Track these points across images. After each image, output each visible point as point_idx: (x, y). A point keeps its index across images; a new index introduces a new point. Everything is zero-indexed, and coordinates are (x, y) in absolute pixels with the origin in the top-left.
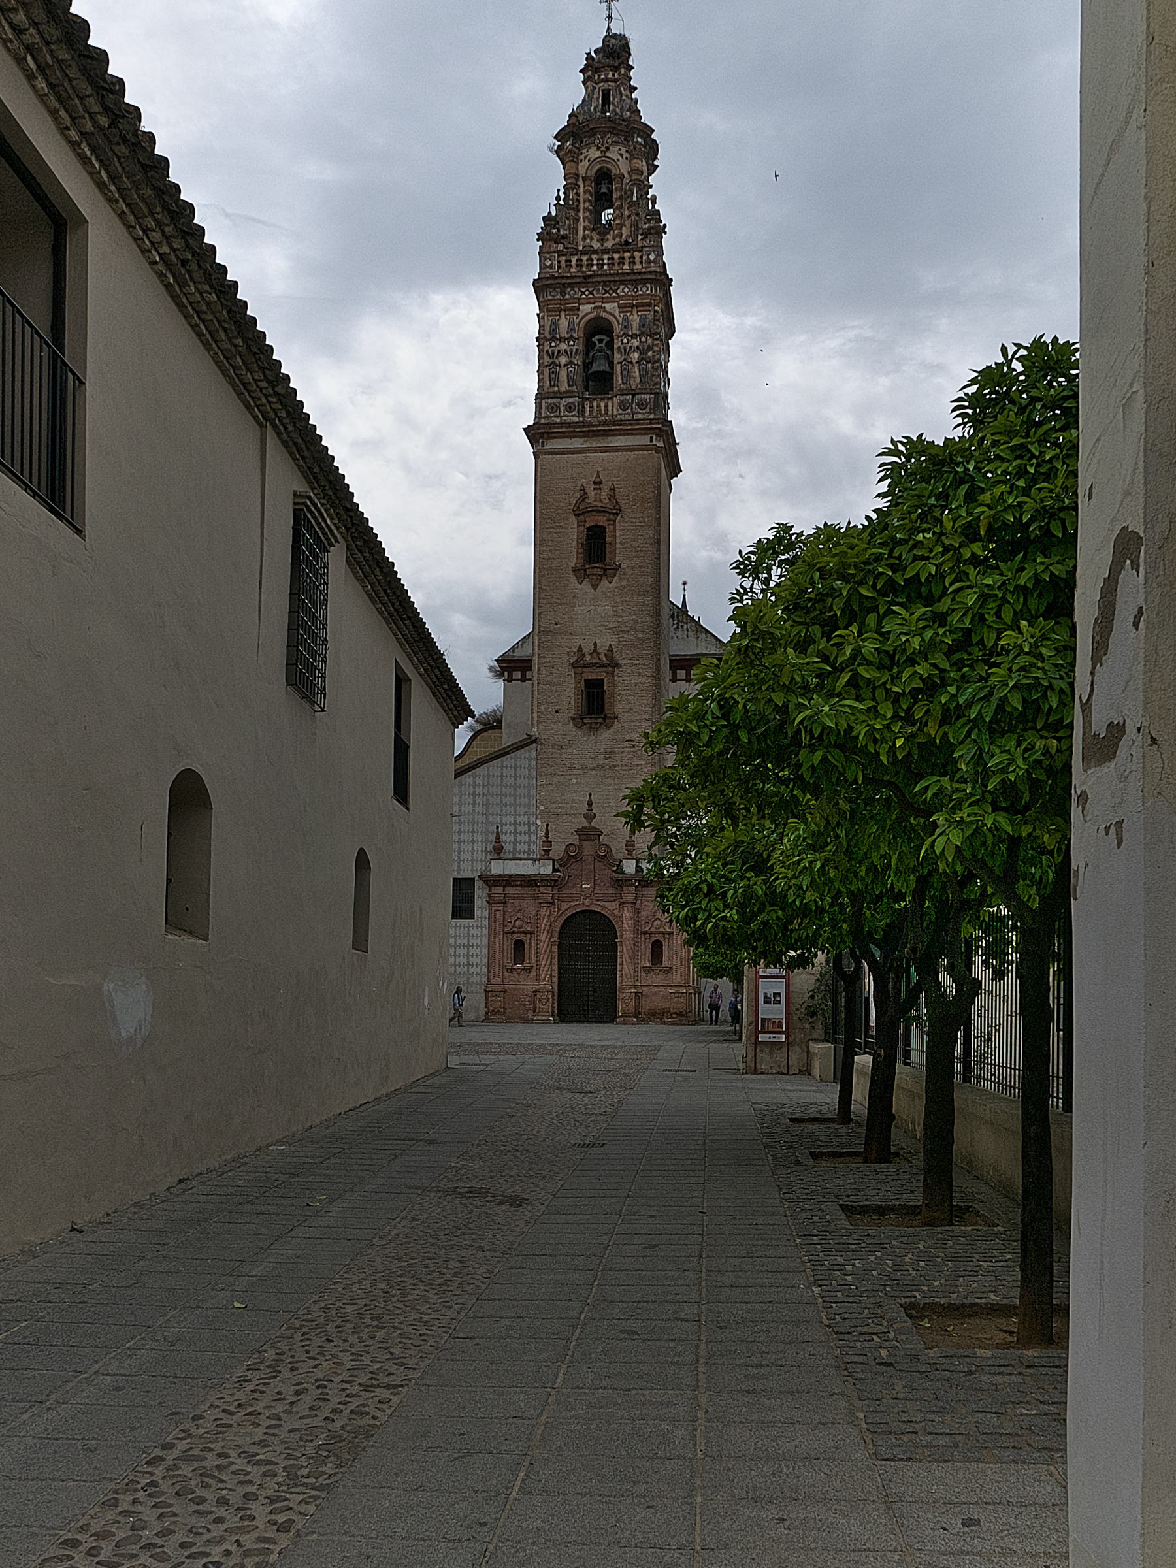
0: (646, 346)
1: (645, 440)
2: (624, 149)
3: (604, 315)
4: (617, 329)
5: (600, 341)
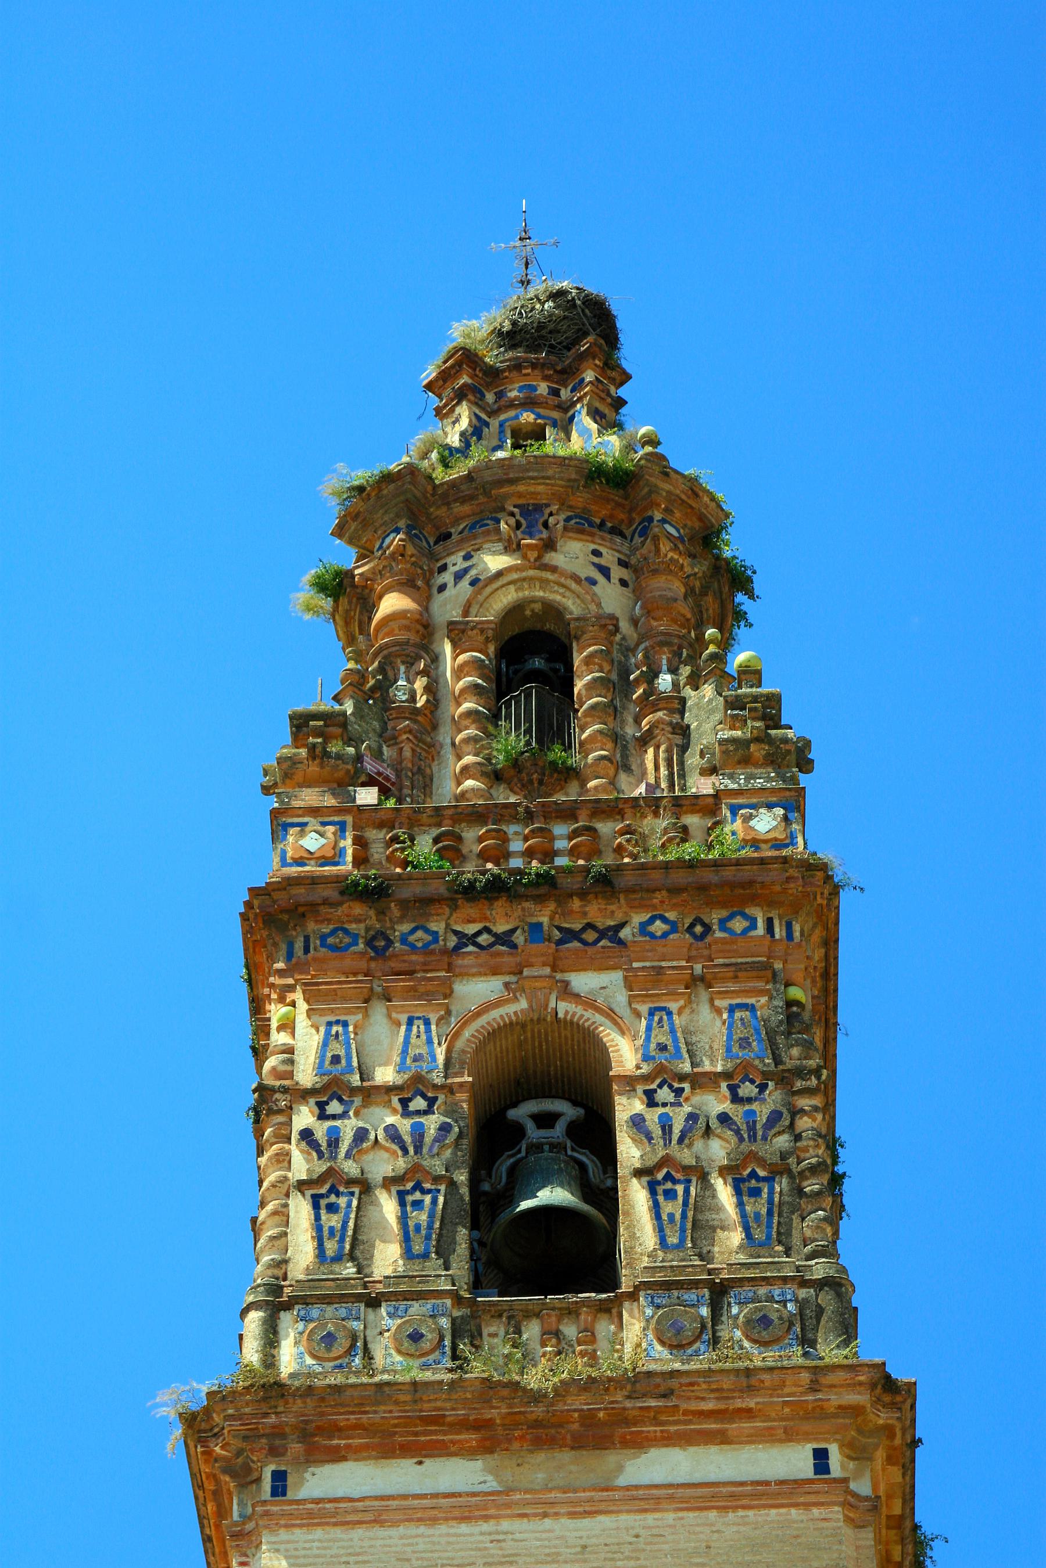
0: (762, 1111)
1: (794, 1461)
2: (609, 558)
3: (564, 1008)
4: (625, 1054)
5: (546, 1120)
